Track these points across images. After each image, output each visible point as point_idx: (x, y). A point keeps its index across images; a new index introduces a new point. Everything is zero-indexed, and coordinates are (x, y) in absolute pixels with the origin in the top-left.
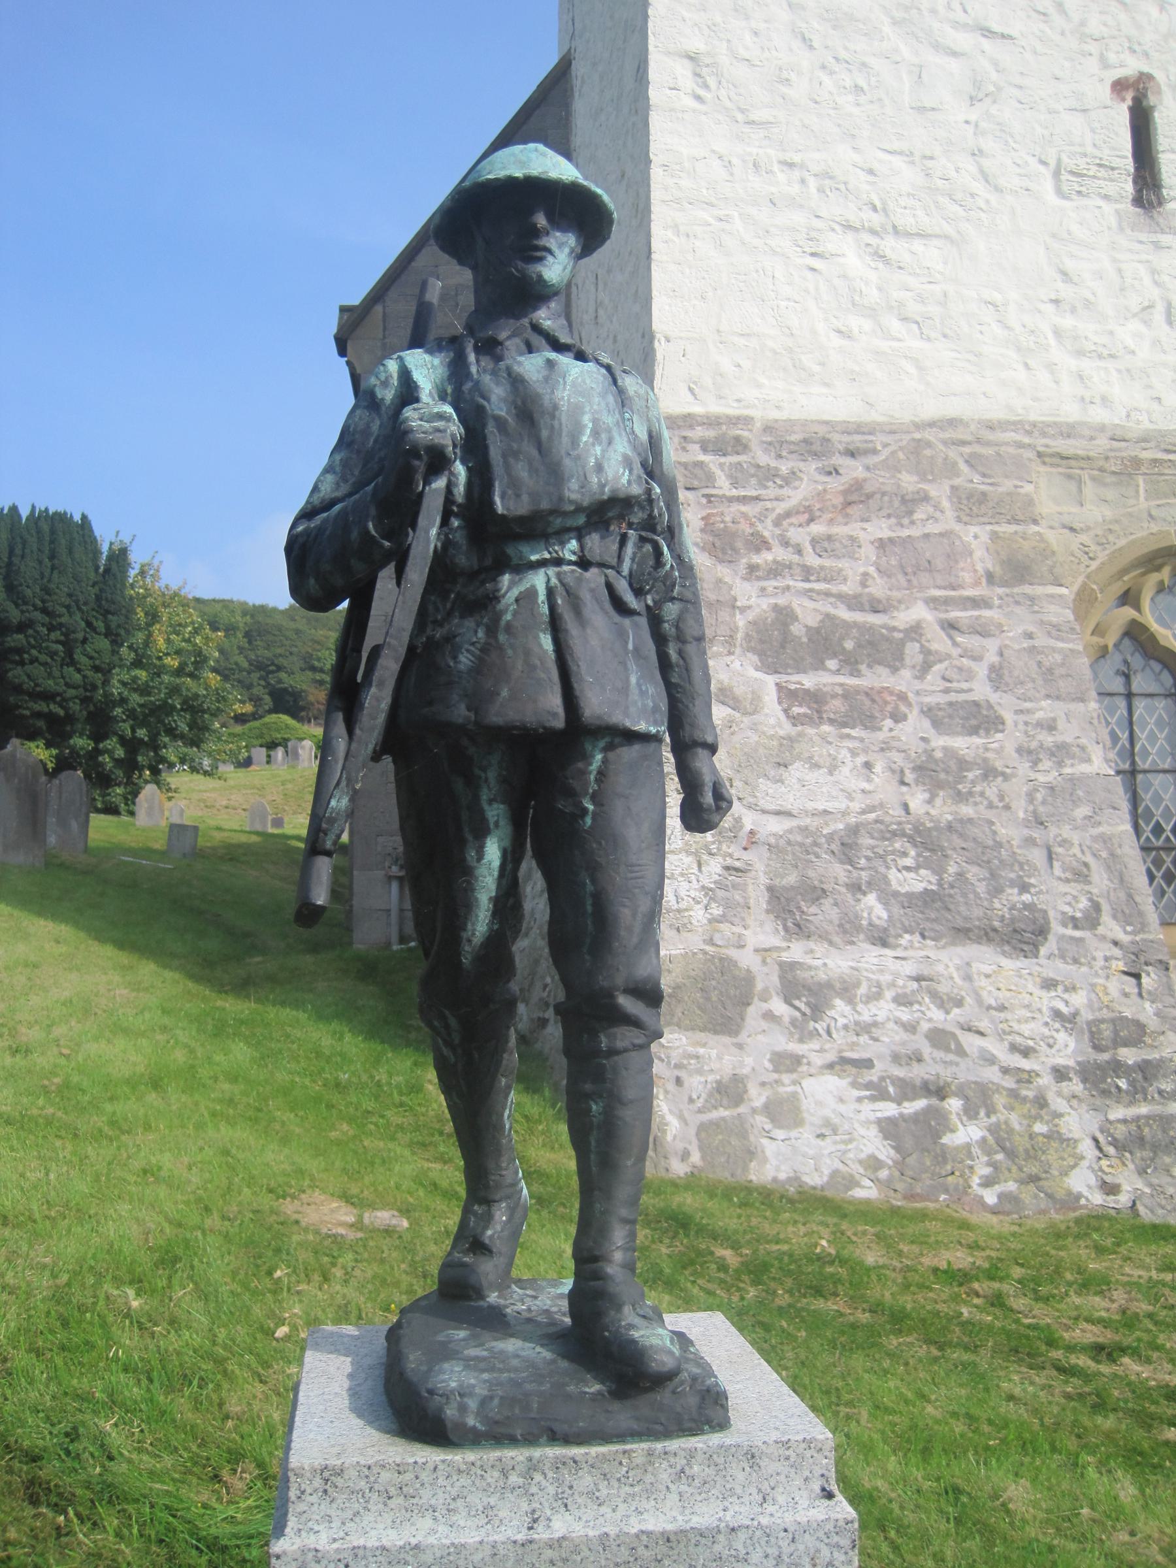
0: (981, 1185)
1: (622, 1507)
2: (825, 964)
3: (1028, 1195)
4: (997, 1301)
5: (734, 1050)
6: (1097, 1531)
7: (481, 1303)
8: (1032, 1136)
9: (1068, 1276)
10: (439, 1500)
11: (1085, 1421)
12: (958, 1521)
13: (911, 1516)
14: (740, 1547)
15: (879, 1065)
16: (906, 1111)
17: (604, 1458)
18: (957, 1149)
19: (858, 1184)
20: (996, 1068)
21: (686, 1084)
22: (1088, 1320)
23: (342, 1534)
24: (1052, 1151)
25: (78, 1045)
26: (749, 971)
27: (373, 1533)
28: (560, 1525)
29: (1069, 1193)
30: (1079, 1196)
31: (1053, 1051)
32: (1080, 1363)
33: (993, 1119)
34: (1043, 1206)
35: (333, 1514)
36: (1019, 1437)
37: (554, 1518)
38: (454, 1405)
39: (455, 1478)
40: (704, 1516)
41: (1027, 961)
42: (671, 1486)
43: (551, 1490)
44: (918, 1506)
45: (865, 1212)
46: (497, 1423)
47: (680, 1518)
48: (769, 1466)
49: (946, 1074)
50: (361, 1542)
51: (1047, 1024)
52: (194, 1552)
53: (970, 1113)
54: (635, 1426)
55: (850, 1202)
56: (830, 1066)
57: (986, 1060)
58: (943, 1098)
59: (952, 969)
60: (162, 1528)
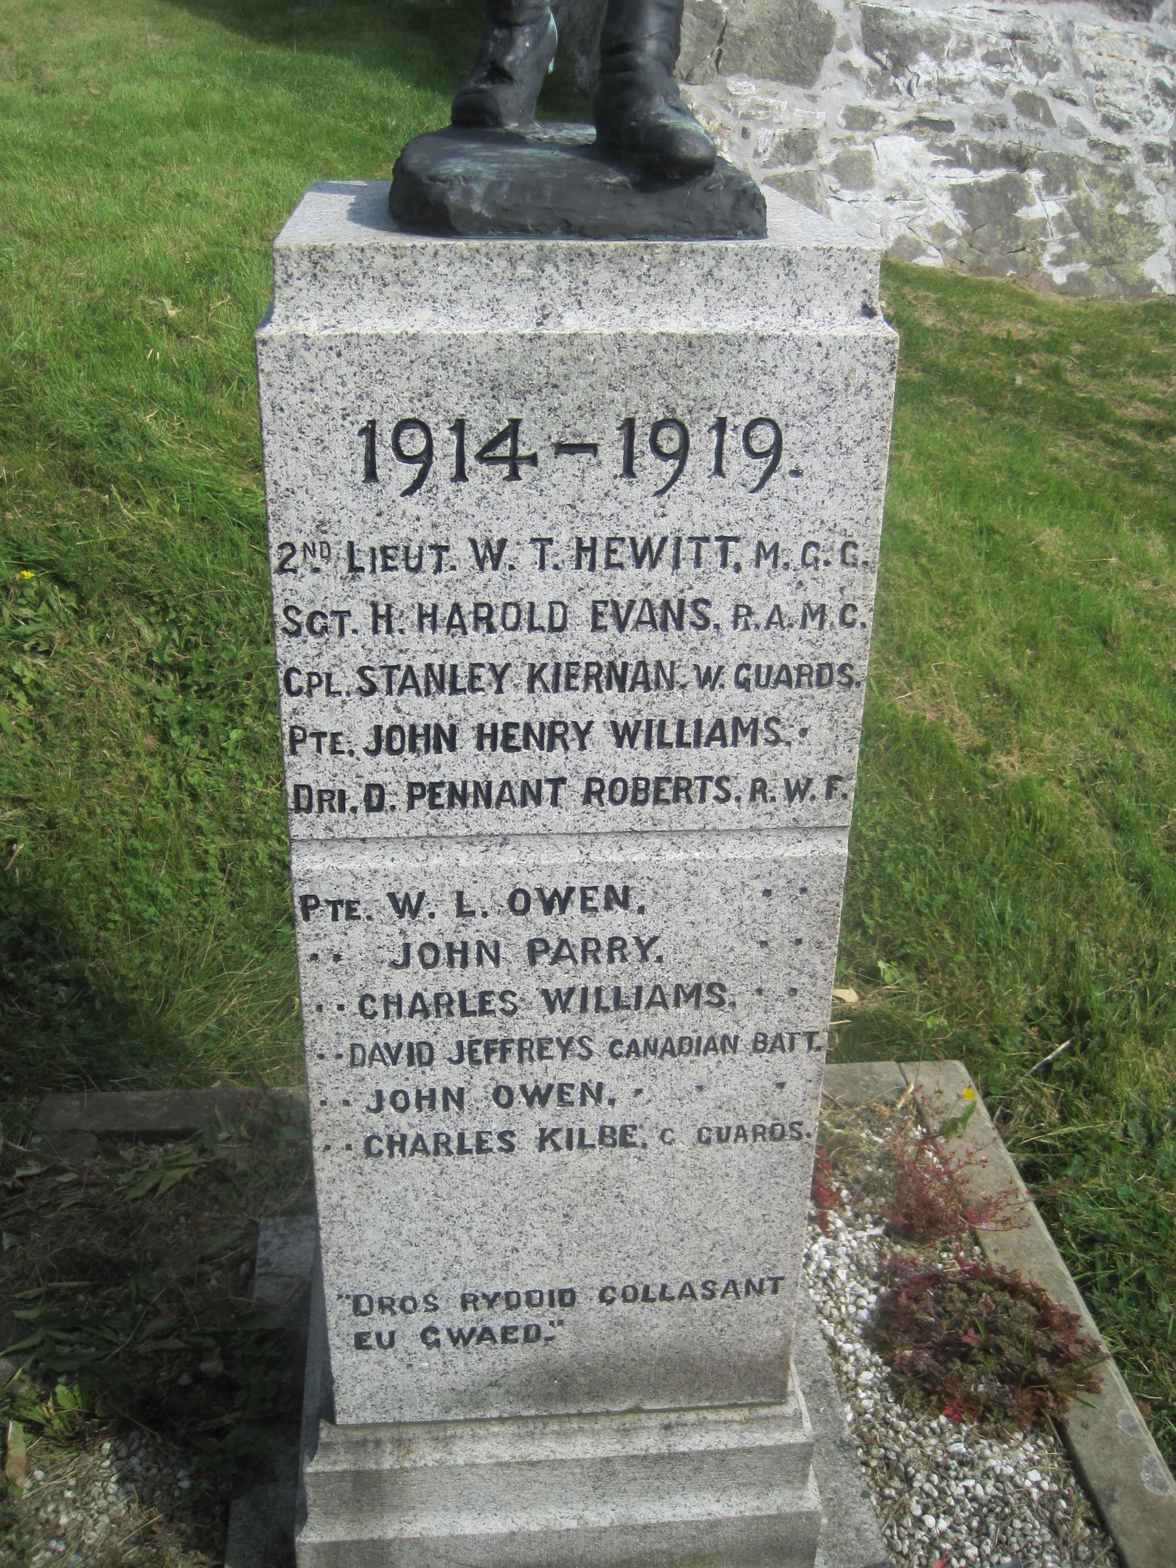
0: (1051, 263)
1: (641, 308)
2: (913, 13)
3: (1098, 278)
4: (1053, 374)
5: (806, 102)
6: (1122, 578)
7: (499, 130)
8: (1111, 217)
9: (1129, 357)
10: (440, 290)
11: (1126, 486)
12: (988, 557)
13: (944, 548)
14: (769, 359)
15: (960, 130)
16: (982, 180)
17: (625, 254)
18: (1032, 224)
19: (923, 252)
20: (1084, 141)
21: (752, 137)
22: (1143, 400)
23: (333, 322)
24: (1130, 235)
25: (109, 86)
26: (829, 16)
27: (368, 321)
28: (572, 322)
29: (1142, 279)
30: (1152, 283)
31: (1149, 127)
32: (1129, 438)
33: (1074, 196)
34: (1112, 291)
35: (324, 301)
36: (1059, 492)
37: (566, 315)
38: (458, 190)
39: (458, 265)
40: (732, 322)
41: (1136, 24)
42: (697, 289)
43: (564, 284)
44: (951, 540)
45: (928, 279)
46: (506, 210)
47: (704, 324)
48: (807, 276)
49: (1030, 142)
50: (355, 330)
51: (1146, 97)
52: (235, 528)
53: (1050, 186)
54: (660, 222)
55: (914, 270)
56: (908, 126)
57: (1075, 132)
58: (1023, 169)
59: (1052, 28)
60: (203, 509)
